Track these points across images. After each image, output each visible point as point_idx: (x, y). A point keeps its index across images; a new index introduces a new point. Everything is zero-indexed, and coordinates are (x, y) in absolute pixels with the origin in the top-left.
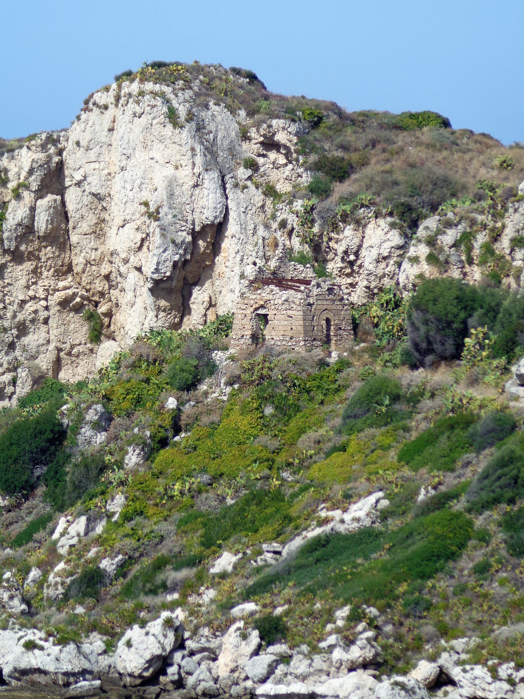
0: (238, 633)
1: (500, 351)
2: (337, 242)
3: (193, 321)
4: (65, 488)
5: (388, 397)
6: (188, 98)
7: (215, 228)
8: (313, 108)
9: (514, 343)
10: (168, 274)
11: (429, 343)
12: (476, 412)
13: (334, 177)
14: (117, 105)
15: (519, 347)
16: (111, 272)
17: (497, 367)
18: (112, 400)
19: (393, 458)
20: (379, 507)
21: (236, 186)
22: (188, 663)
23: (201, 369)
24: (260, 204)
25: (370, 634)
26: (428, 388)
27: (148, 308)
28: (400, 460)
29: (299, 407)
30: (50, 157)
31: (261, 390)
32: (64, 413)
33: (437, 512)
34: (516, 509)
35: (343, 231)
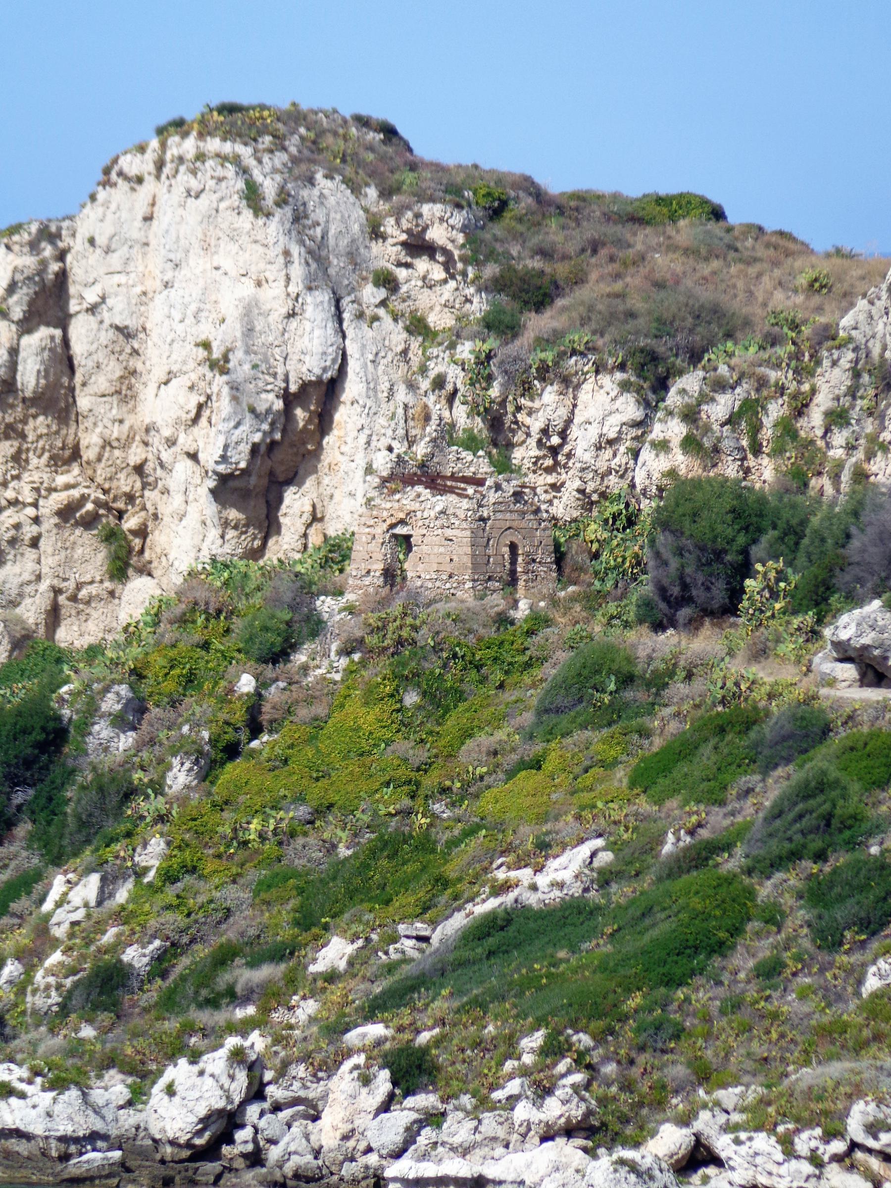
0: (355, 1074)
1: (805, 602)
2: (529, 414)
3: (285, 545)
4: (64, 825)
5: (613, 678)
6: (278, 165)
7: (324, 388)
8: (492, 184)
9: (828, 589)
10: (243, 465)
11: (685, 587)
13: (526, 303)
14: (158, 177)
15: (837, 596)
16: (146, 460)
17: (799, 629)
18: (145, 677)
20: (596, 864)
21: (360, 316)
22: (270, 1124)
23: (296, 626)
24: (400, 348)
25: (578, 1077)
26: (682, 663)
27: (208, 522)
28: (633, 784)
29: (462, 692)
30: (44, 263)
31: (399, 662)
32: (63, 699)
34: (827, 869)
35: (540, 395)
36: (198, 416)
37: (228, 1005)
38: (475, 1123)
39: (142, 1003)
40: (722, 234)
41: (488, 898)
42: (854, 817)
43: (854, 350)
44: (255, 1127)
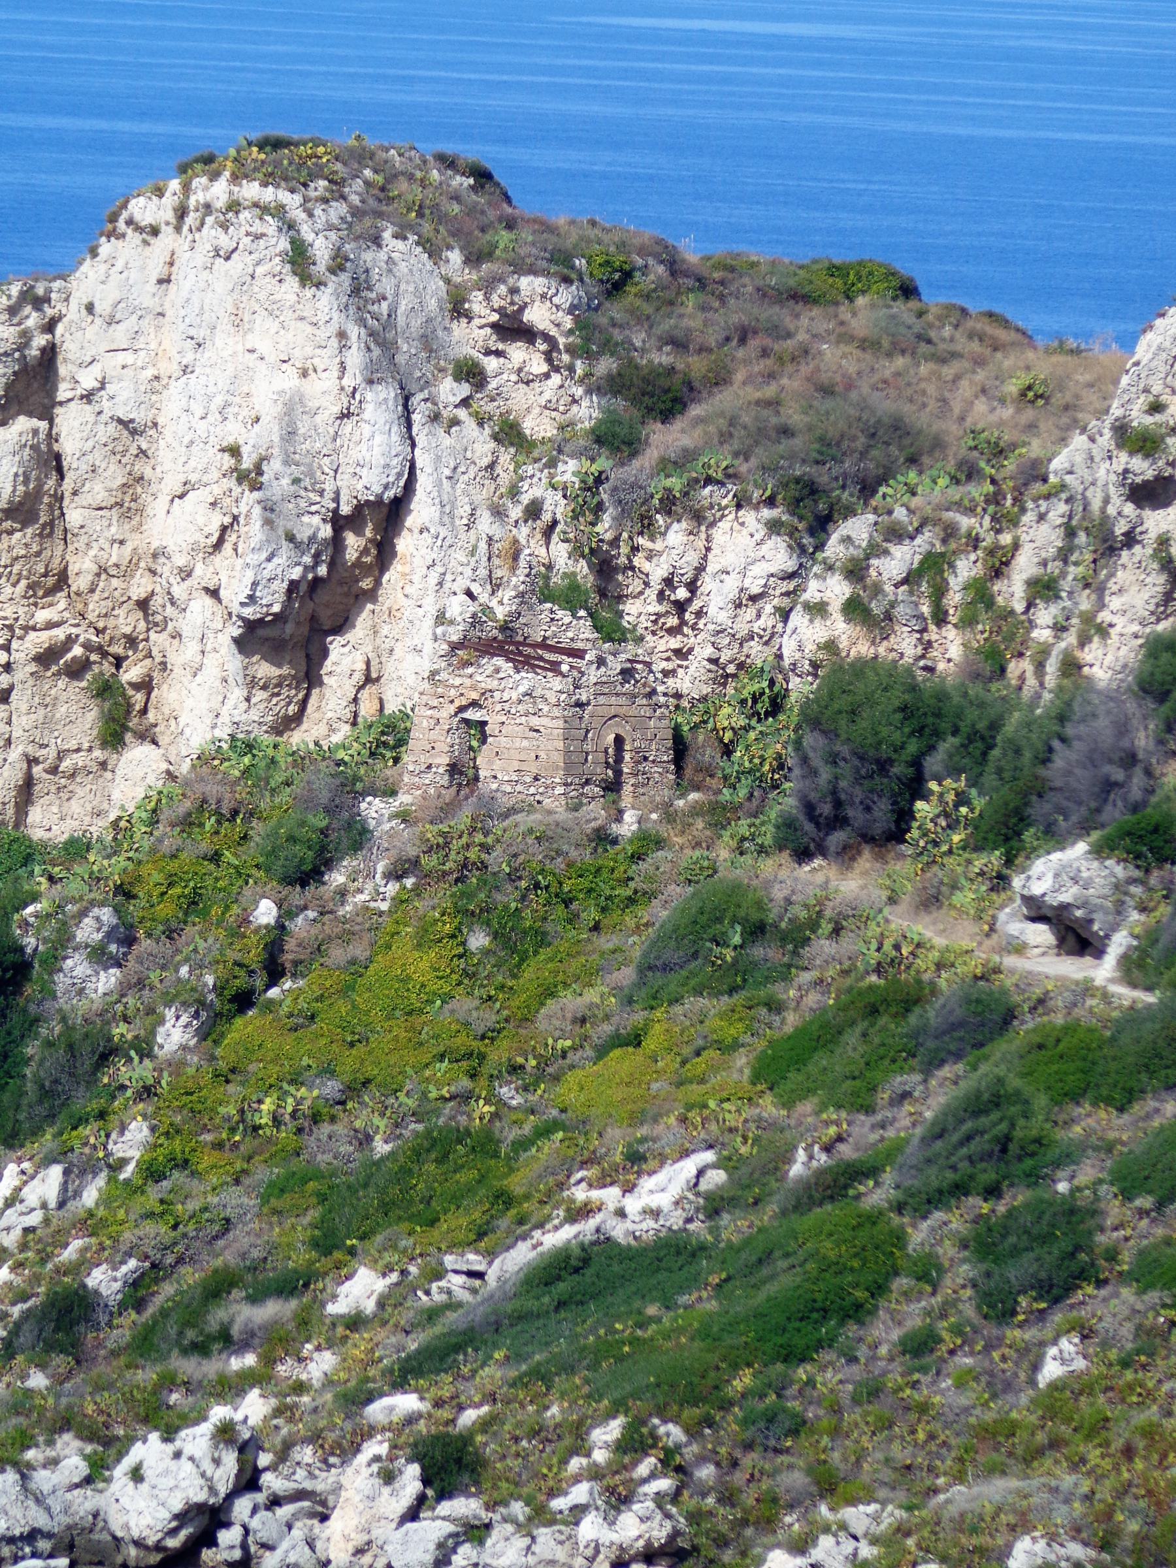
0: (375, 1467)
1: (991, 836)
2: (649, 558)
3: (327, 723)
5: (738, 928)
6: (336, 221)
7: (385, 510)
9: (1022, 820)
10: (276, 609)
11: (838, 804)
12: (926, 977)
13: (650, 410)
14: (178, 229)
16: (153, 593)
17: (982, 874)
18: (135, 897)
19: (741, 1071)
20: (703, 1186)
21: (435, 418)
22: (264, 1524)
23: (334, 836)
24: (486, 461)
25: (664, 1484)
26: (828, 913)
28: (755, 1079)
29: (545, 934)
30: (26, 336)
31: (463, 894)
32: (27, 924)
33: (829, 1207)
34: (1001, 1209)
35: (664, 534)
36: (221, 541)
37: (220, 1352)
38: (527, 1540)
39: (110, 1344)
40: (909, 319)
41: (561, 1225)
42: (1038, 1141)
43: (1067, 501)
44: (247, 1531)
